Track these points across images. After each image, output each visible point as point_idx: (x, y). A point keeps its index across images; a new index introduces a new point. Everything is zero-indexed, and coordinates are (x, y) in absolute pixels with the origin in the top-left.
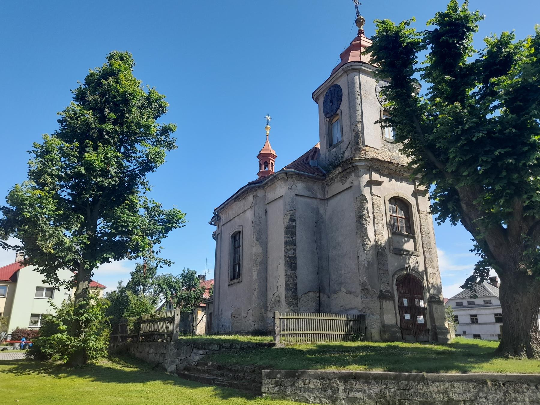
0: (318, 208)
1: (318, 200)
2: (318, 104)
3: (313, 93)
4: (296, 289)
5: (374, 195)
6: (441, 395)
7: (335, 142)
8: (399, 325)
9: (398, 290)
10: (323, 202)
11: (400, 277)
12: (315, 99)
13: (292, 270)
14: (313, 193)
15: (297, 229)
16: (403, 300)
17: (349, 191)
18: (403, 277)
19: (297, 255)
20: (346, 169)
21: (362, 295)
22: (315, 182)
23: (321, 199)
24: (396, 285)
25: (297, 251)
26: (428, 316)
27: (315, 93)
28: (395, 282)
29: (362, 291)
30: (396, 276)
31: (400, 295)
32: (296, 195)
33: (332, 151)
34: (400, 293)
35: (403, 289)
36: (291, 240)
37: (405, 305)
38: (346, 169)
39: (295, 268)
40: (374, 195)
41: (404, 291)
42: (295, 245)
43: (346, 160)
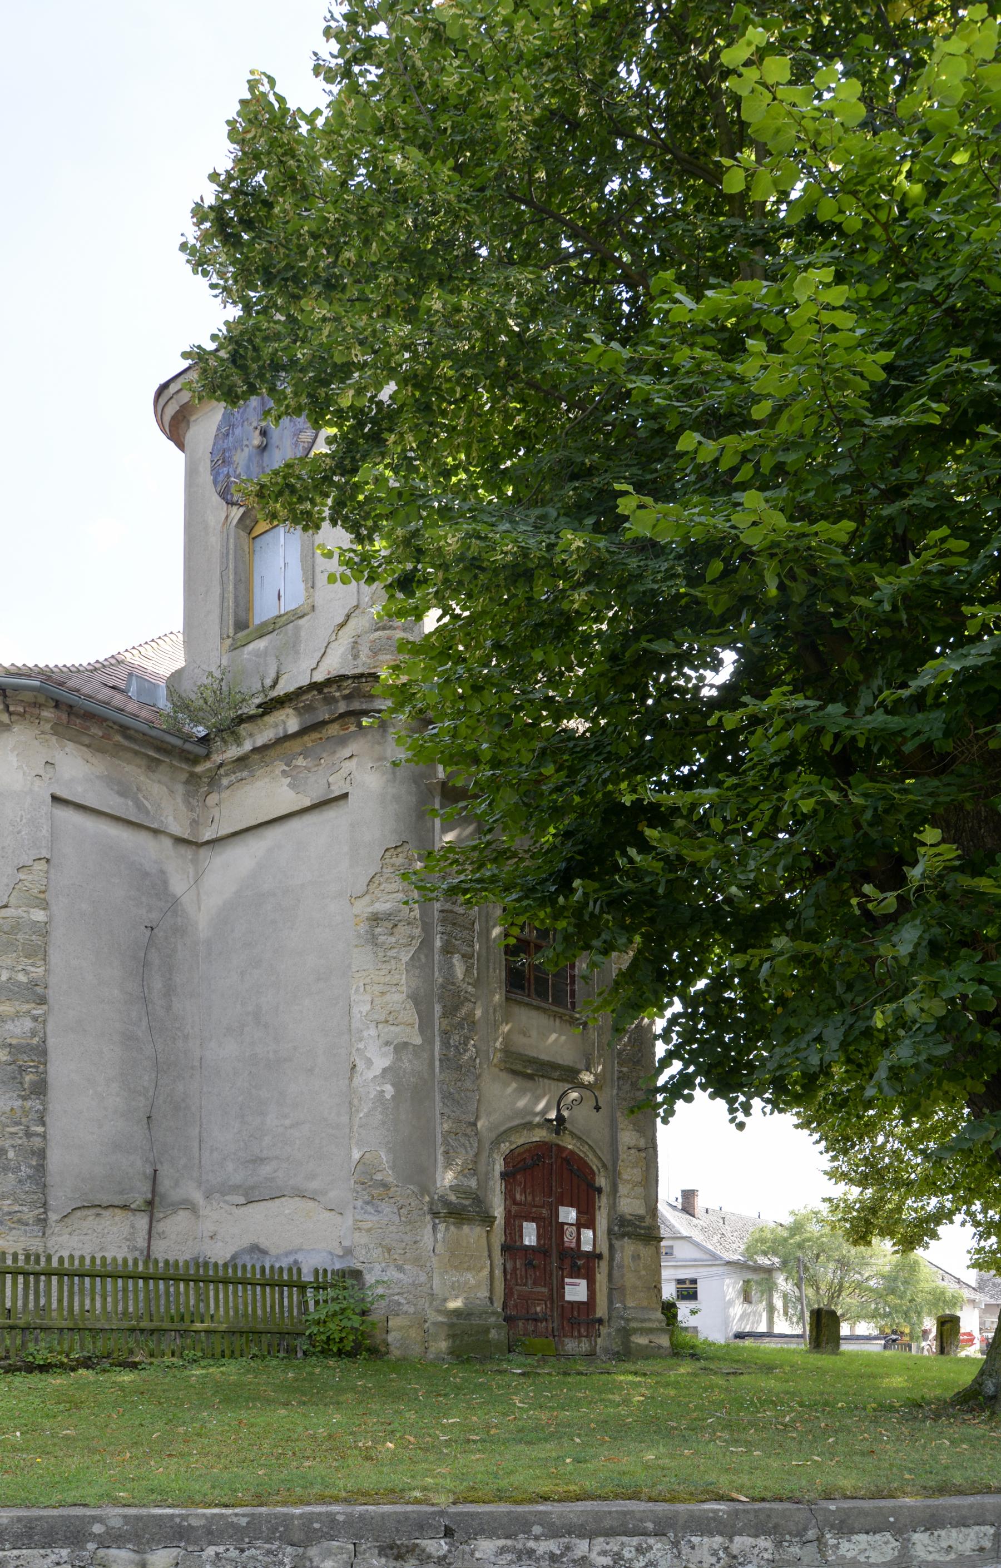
0: (163, 872)
1: (168, 842)
2: (181, 445)
3: (164, 387)
4: (41, 1168)
5: (843, 308)
6: (182, 1285)
7: (264, 609)
8: (498, 1306)
9: (509, 1195)
10: (188, 852)
11: (521, 1150)
12: (167, 418)
13: (24, 1098)
14: (140, 806)
15: (58, 935)
16: (521, 1227)
17: (330, 814)
18: (526, 1151)
19: (51, 1042)
20: (324, 723)
21: (359, 1203)
22: (152, 765)
23: (180, 841)
24: (504, 1175)
25: (50, 1027)
26: (601, 1278)
27: (173, 388)
28: (499, 1166)
29: (359, 1187)
30: (505, 1147)
31: (514, 1209)
32: (55, 799)
33: (251, 647)
34: (515, 1202)
35: (524, 1191)
36: (22, 978)
37: (527, 1242)
38: (324, 723)
39: (40, 1089)
40: (843, 308)
41: (529, 1198)
42: (42, 1000)
43: (329, 682)
